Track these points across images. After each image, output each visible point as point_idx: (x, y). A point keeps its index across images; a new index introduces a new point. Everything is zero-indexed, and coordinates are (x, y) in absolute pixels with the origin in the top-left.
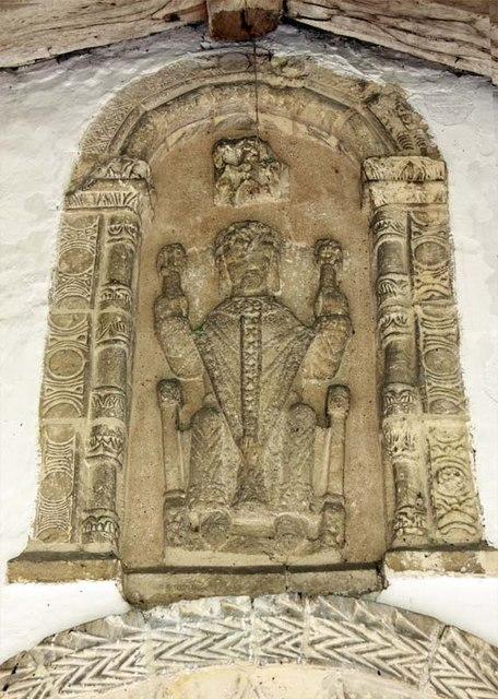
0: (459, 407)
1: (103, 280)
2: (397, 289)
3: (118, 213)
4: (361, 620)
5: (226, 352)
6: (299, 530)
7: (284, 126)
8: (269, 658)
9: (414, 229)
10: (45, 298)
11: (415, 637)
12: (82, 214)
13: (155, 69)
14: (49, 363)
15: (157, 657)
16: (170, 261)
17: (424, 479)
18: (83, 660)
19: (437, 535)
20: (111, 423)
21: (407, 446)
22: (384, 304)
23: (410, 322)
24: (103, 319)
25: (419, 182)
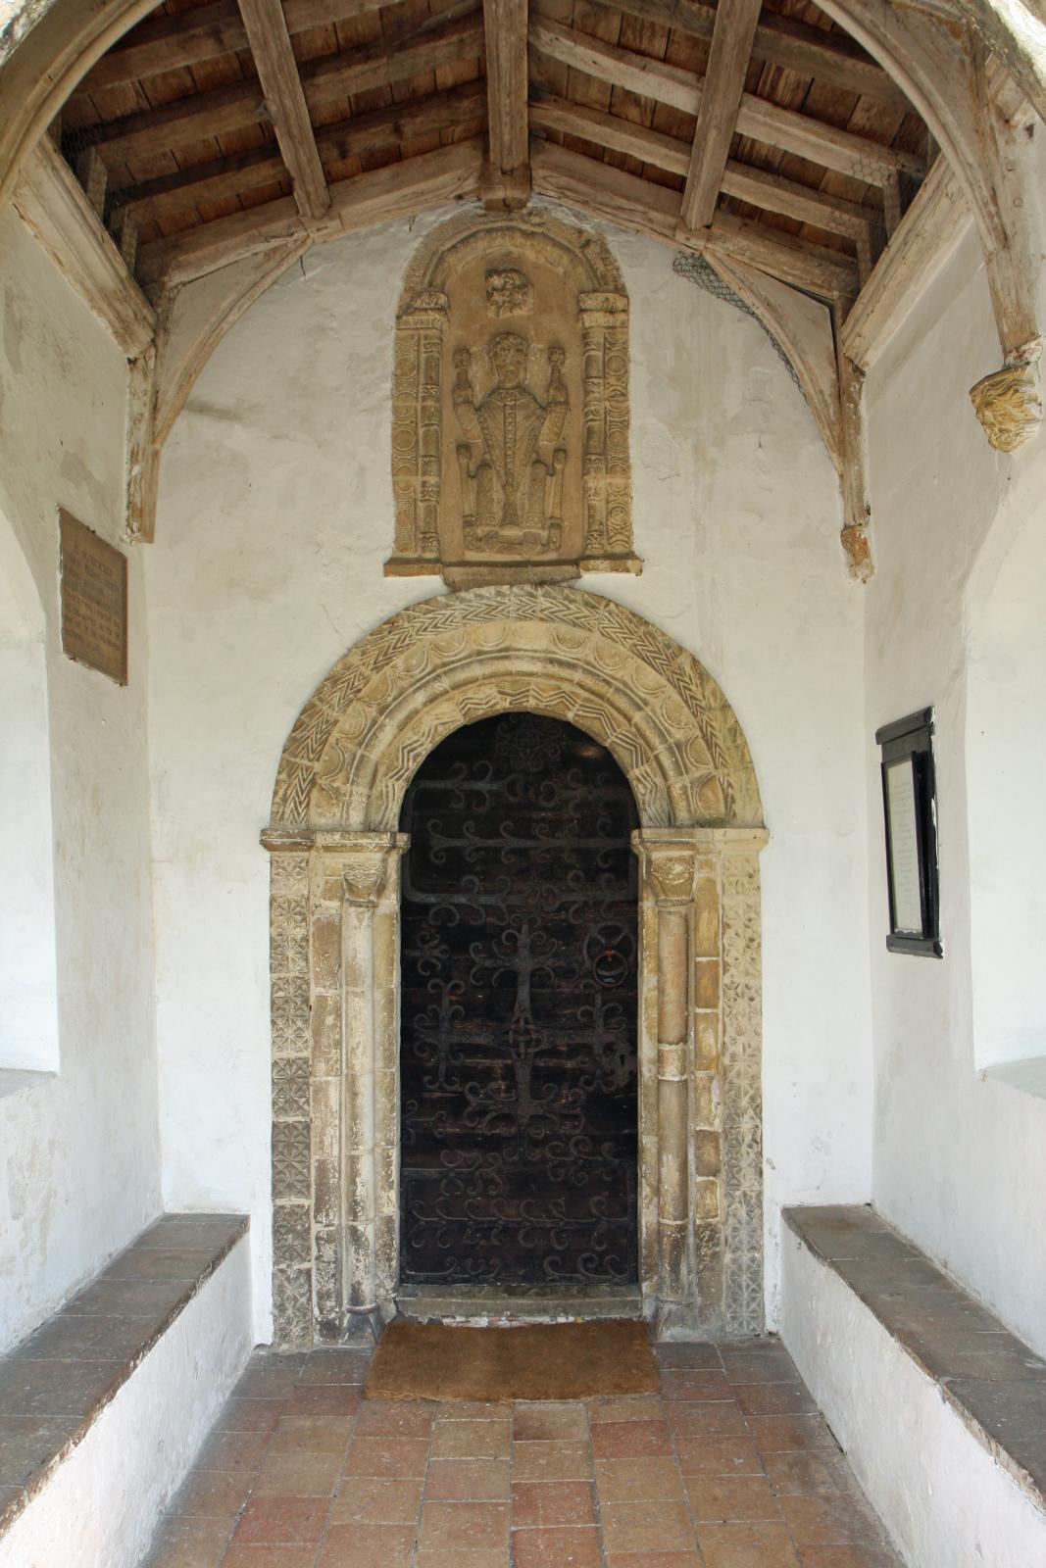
0: (626, 470)
1: (422, 381)
2: (596, 389)
3: (429, 332)
4: (566, 598)
6: (536, 539)
7: (530, 255)
8: (520, 618)
9: (608, 345)
10: (389, 393)
11: (593, 607)
12: (405, 332)
13: (448, 217)
14: (395, 438)
15: (464, 617)
16: (461, 361)
17: (604, 513)
18: (426, 619)
19: (608, 548)
21: (596, 494)
22: (588, 399)
23: (602, 412)
24: (424, 408)
25: (612, 312)
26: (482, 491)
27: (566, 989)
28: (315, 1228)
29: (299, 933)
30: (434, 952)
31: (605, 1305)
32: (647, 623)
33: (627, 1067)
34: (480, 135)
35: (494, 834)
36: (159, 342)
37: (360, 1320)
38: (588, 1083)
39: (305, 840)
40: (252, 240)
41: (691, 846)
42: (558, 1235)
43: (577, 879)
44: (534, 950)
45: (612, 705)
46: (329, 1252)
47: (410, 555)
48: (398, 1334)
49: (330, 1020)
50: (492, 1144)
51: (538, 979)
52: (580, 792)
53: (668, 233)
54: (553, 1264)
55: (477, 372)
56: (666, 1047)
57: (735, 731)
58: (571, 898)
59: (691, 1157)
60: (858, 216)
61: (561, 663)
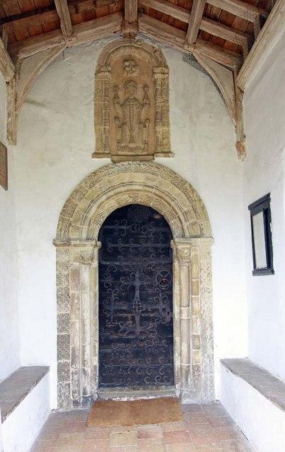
5: (127, 111)
7: (137, 55)
8: (136, 172)
14: (95, 114)
20: (108, 127)
26: (123, 131)
27: (150, 291)
28: (71, 370)
29: (66, 273)
30: (109, 280)
31: (164, 392)
32: (175, 174)
33: (170, 316)
34: (122, 11)
35: (127, 242)
36: (17, 77)
37: (86, 399)
38: (158, 321)
39: (67, 243)
40: (47, 44)
41: (190, 244)
42: (149, 370)
43: (153, 256)
44: (140, 279)
45: (165, 200)
46: (76, 377)
47: (100, 151)
48: (98, 404)
49: (76, 301)
50: (128, 341)
51: (142, 288)
52: (154, 229)
53: (182, 45)
54: (147, 380)
55: (121, 94)
56: (182, 308)
57: (203, 208)
58: (152, 262)
59: (191, 343)
60: (244, 35)
61: (149, 186)
